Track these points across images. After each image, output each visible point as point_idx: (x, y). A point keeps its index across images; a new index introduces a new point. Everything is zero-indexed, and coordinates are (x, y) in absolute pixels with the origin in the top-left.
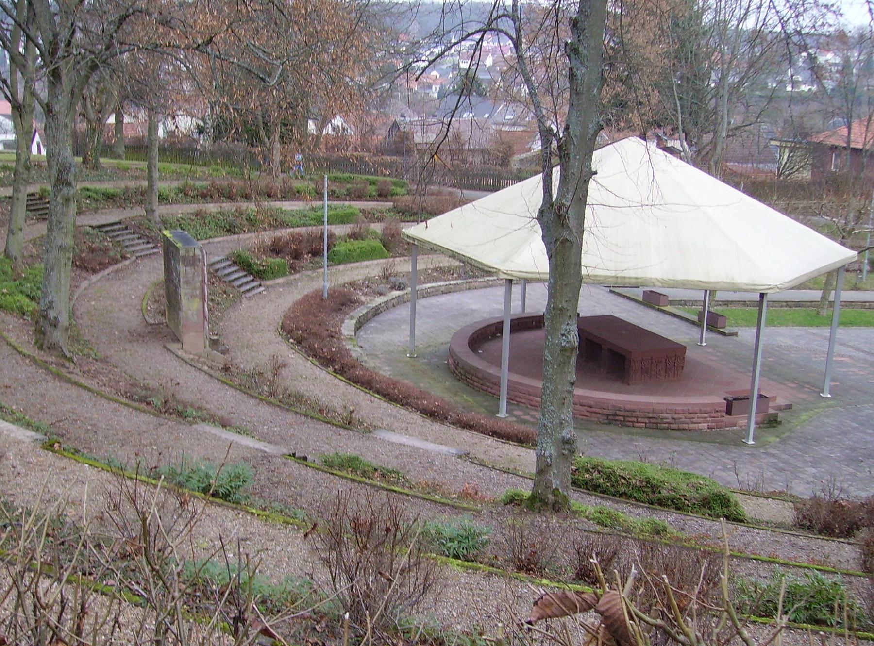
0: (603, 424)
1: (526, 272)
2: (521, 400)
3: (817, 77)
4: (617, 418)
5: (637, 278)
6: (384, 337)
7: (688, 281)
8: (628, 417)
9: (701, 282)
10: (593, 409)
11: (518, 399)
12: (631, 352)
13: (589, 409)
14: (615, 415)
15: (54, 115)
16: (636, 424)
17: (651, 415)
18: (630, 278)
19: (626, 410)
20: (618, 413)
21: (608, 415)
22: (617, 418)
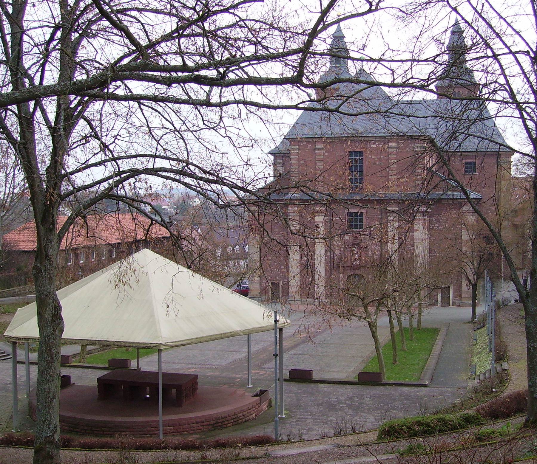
0: (212, 431)
1: (176, 342)
2: (153, 432)
3: (335, 201)
4: (218, 425)
5: (231, 332)
6: (518, 420)
7: (254, 328)
8: (223, 422)
9: (260, 327)
10: (205, 423)
11: (151, 433)
12: (97, 379)
13: (202, 424)
14: (217, 423)
15: (50, 258)
16: (228, 425)
17: (234, 417)
18: (227, 333)
19: (222, 418)
20: (219, 421)
21: (213, 424)
22: (218, 425)
